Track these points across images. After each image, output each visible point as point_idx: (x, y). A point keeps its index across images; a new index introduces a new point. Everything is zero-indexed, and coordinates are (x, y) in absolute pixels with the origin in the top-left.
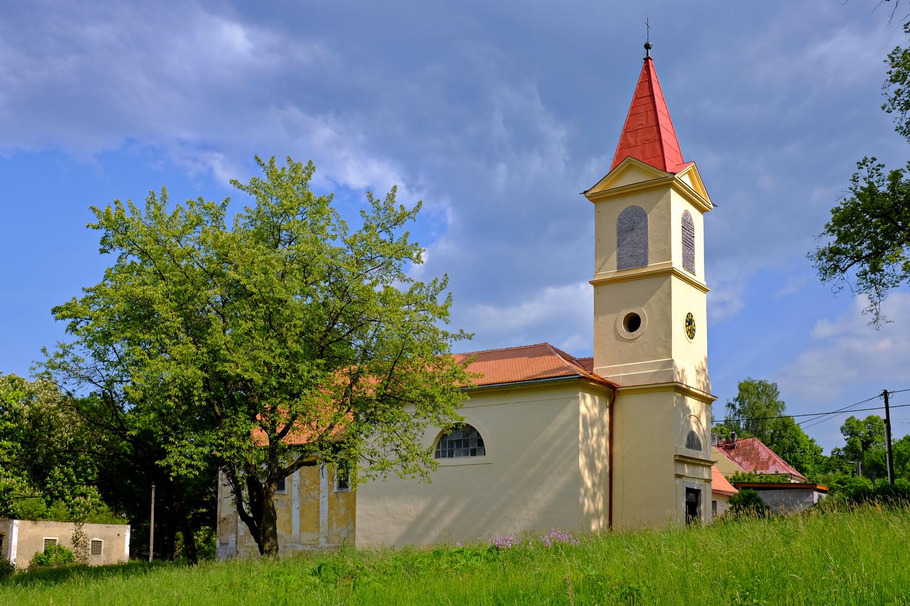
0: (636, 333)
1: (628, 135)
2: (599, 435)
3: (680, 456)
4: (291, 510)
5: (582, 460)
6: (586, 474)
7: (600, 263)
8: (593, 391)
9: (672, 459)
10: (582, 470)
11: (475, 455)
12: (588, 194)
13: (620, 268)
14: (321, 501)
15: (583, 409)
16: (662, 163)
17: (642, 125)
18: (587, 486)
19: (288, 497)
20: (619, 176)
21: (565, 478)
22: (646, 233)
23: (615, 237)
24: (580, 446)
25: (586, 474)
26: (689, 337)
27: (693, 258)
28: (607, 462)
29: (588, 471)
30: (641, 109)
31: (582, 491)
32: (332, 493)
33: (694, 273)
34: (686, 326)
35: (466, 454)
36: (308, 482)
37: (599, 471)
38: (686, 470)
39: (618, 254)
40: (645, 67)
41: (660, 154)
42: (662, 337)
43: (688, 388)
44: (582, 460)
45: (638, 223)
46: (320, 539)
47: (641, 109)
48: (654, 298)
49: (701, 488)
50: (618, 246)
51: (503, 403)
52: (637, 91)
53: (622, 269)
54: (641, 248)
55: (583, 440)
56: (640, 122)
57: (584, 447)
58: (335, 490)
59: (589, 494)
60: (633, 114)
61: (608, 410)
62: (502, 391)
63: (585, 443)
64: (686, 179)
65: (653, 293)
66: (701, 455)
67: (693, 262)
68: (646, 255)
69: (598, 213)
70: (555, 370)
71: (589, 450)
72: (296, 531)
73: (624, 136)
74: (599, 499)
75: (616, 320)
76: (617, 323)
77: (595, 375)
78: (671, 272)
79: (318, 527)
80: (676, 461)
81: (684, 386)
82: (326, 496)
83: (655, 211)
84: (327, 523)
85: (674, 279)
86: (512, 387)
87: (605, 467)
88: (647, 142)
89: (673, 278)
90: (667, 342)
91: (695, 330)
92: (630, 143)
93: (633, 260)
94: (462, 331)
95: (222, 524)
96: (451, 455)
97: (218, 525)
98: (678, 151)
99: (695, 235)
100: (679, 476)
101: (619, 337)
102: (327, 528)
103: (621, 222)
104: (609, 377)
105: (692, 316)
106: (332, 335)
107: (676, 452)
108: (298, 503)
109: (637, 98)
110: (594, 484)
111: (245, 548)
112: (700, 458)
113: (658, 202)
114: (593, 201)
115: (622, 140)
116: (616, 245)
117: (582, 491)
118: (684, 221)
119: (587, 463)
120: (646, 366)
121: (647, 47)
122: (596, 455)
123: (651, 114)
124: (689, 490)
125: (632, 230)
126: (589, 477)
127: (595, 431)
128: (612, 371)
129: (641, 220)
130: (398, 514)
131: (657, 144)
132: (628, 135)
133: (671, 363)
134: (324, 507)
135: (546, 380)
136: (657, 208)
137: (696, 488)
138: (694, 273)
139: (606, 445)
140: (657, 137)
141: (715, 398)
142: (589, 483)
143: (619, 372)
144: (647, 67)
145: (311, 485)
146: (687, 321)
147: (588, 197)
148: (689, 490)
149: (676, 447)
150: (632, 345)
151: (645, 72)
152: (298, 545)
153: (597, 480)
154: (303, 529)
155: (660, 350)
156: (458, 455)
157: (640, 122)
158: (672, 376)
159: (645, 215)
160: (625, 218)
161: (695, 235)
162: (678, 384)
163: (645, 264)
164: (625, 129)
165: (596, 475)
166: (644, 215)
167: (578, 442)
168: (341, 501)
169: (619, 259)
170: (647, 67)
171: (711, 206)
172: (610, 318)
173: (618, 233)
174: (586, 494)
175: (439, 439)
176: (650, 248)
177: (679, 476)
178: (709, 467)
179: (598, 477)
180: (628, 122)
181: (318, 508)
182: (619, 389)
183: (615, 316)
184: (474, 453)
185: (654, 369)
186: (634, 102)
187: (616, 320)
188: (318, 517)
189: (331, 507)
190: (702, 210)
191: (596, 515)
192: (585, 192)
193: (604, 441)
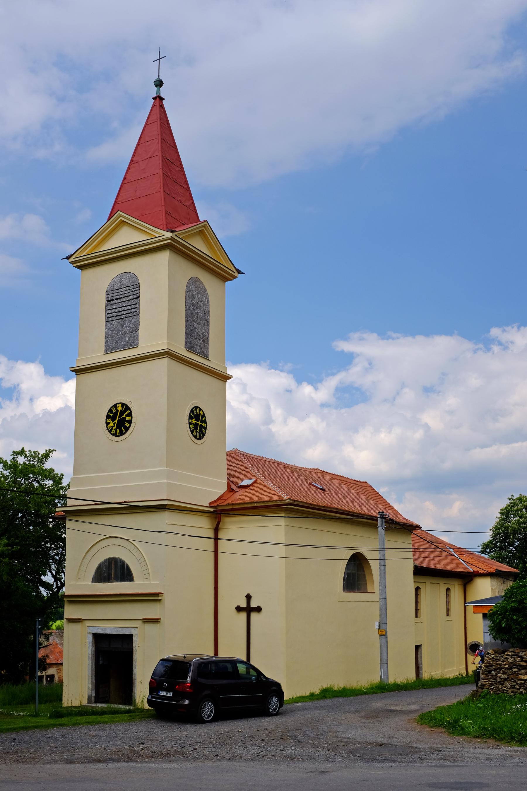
12: (72, 259)
13: (109, 350)
26: (196, 437)
33: (206, 357)
49: (133, 632)
91: (205, 428)
138: (206, 357)
163: (133, 344)
192: (68, 258)
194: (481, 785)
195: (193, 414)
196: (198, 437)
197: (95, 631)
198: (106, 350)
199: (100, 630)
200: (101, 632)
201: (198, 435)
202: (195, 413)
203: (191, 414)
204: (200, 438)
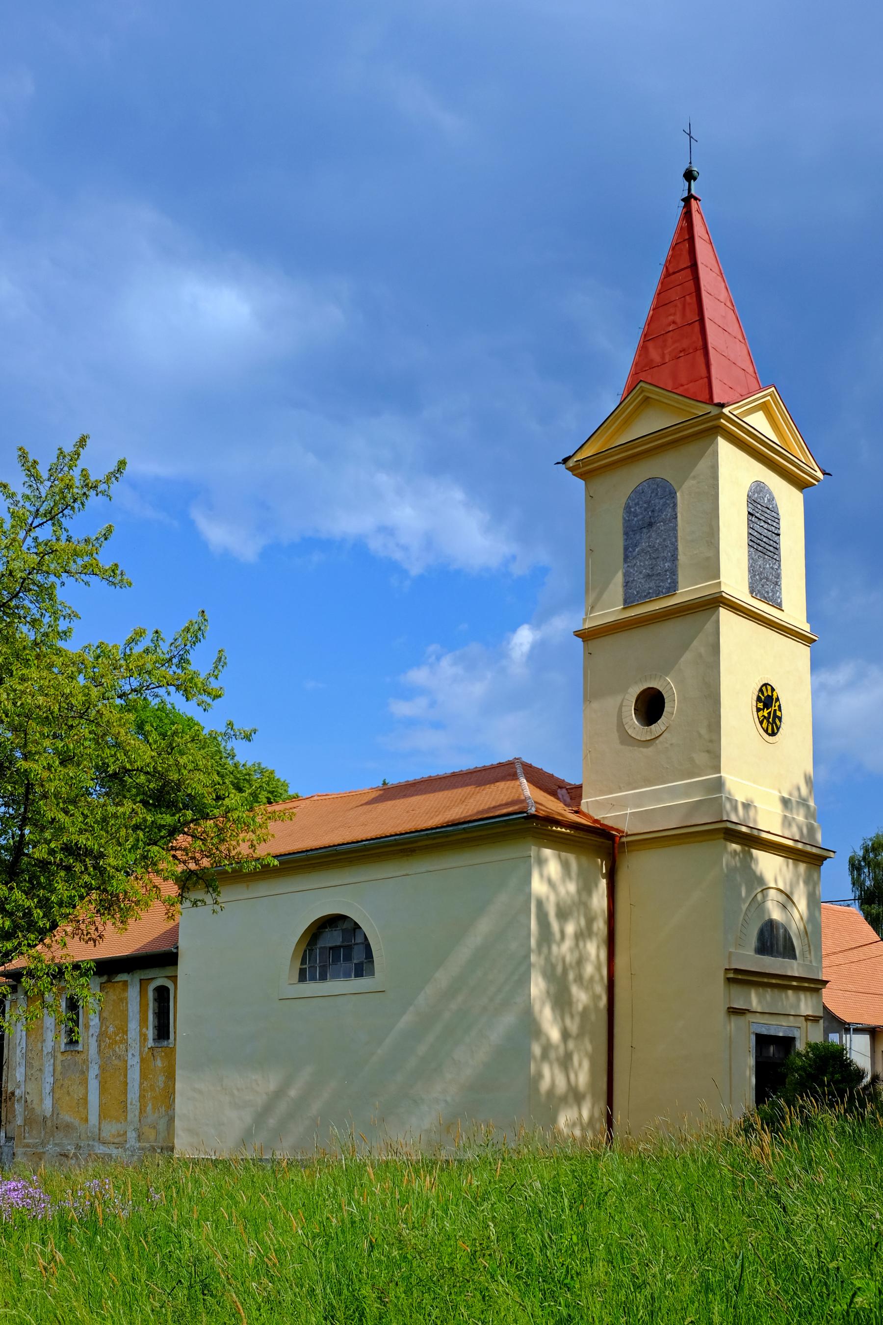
0: (657, 728)
1: (650, 345)
2: (580, 936)
3: (736, 971)
4: (87, 1079)
5: (537, 986)
6: (546, 1016)
7: (592, 597)
8: (559, 843)
9: (721, 977)
10: (537, 1007)
11: (362, 976)
12: (571, 463)
13: (628, 603)
14: (130, 1063)
15: (538, 886)
16: (707, 391)
17: (674, 322)
18: (548, 1039)
19: (83, 1056)
20: (628, 422)
21: (509, 1019)
22: (675, 529)
23: (619, 542)
24: (533, 958)
25: (546, 1016)
26: (766, 731)
27: (778, 576)
28: (600, 990)
29: (553, 1010)
30: (674, 295)
31: (537, 1050)
32: (146, 1049)
33: (779, 607)
34: (758, 710)
35: (347, 975)
36: (111, 1030)
37: (580, 1007)
38: (755, 1000)
39: (625, 575)
40: (685, 213)
41: (704, 373)
42: (703, 731)
43: (755, 832)
44: (537, 986)
45: (661, 511)
46: (129, 1134)
47: (674, 295)
48: (688, 656)
49: (796, 1034)
50: (626, 558)
51: (404, 873)
52: (669, 262)
53: (633, 602)
54: (665, 559)
55: (539, 945)
56: (671, 318)
57: (542, 962)
58: (150, 1043)
59: (553, 1055)
60: (661, 305)
61: (603, 883)
62: (402, 851)
63: (545, 950)
64: (759, 422)
65: (685, 646)
66: (794, 969)
67: (777, 584)
68: (674, 572)
69: (590, 497)
70: (494, 807)
71: (553, 967)
72: (93, 1119)
73: (643, 349)
74: (580, 1064)
75: (621, 706)
76: (624, 709)
77: (585, 815)
78: (718, 601)
79: (125, 1111)
80: (729, 980)
81: (744, 829)
82: (137, 1054)
83: (690, 483)
84: (138, 1104)
85: (724, 614)
86: (416, 842)
87: (596, 998)
88: (682, 354)
89: (724, 613)
90: (711, 741)
91: (780, 719)
92: (652, 361)
93: (652, 584)
94: (230, 725)
95: (9, 1103)
96: (323, 978)
97: (3, 1105)
98: (750, 370)
99: (782, 532)
100: (733, 1012)
101: (627, 739)
102: (137, 1113)
103: (629, 512)
104: (607, 816)
105: (773, 690)
106: (52, 754)
107: (729, 963)
108: (96, 1067)
109: (668, 274)
110: (565, 1035)
111: (23, 1147)
112: (789, 973)
113: (695, 465)
114: (581, 476)
115: (640, 356)
116: (622, 557)
117: (537, 1050)
118: (752, 501)
119: (548, 992)
120: (673, 792)
121: (689, 176)
122: (571, 976)
123: (691, 300)
124: (763, 1041)
125: (651, 525)
126: (555, 1018)
127: (570, 929)
128: (613, 805)
129: (665, 504)
130: (238, 1090)
131: (700, 354)
132: (650, 345)
133: (719, 785)
134: (134, 1075)
135: (471, 825)
136: (694, 478)
137: (781, 1034)
138: (779, 607)
139: (598, 956)
140: (700, 343)
141: (825, 853)
142: (554, 1034)
143: (625, 807)
144: (688, 215)
145: (116, 1034)
146: (759, 699)
147: (569, 469)
148: (763, 1041)
149: (730, 953)
150: (649, 751)
151: (685, 224)
152: (96, 1144)
153: (573, 1026)
154: (103, 1115)
155: (701, 758)
156: (335, 976)
157: (671, 318)
158: (721, 808)
159: (672, 495)
160: (637, 504)
161: (782, 532)
162: (729, 825)
163: (672, 589)
164: (645, 336)
165: (572, 1016)
166: (670, 493)
167: (529, 951)
168: (159, 1063)
169: (626, 584)
170: (688, 215)
171: (819, 474)
172: (611, 703)
173: (626, 534)
174: (545, 1056)
175: (304, 946)
176: (682, 558)
177: (733, 1012)
178: (817, 990)
179: (577, 1019)
180: (651, 321)
181: (126, 1076)
182: (624, 840)
183: (619, 699)
184: (359, 973)
185: (689, 797)
186: (663, 283)
187: (621, 706)
188: (126, 1094)
189: (143, 1076)
190: (800, 485)
191: (575, 1096)
192: (565, 461)
193: (595, 950)
194: (3, 1012)
195: (763, 694)
196: (770, 731)
197: (758, 1031)
198: (625, 602)
199: (764, 1029)
200: (765, 1033)
201: (770, 728)
202: (766, 694)
203: (760, 695)
204: (773, 734)
